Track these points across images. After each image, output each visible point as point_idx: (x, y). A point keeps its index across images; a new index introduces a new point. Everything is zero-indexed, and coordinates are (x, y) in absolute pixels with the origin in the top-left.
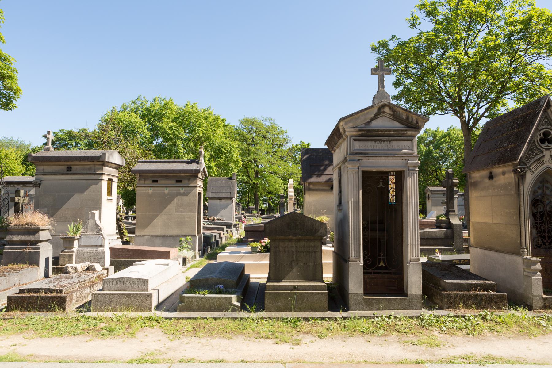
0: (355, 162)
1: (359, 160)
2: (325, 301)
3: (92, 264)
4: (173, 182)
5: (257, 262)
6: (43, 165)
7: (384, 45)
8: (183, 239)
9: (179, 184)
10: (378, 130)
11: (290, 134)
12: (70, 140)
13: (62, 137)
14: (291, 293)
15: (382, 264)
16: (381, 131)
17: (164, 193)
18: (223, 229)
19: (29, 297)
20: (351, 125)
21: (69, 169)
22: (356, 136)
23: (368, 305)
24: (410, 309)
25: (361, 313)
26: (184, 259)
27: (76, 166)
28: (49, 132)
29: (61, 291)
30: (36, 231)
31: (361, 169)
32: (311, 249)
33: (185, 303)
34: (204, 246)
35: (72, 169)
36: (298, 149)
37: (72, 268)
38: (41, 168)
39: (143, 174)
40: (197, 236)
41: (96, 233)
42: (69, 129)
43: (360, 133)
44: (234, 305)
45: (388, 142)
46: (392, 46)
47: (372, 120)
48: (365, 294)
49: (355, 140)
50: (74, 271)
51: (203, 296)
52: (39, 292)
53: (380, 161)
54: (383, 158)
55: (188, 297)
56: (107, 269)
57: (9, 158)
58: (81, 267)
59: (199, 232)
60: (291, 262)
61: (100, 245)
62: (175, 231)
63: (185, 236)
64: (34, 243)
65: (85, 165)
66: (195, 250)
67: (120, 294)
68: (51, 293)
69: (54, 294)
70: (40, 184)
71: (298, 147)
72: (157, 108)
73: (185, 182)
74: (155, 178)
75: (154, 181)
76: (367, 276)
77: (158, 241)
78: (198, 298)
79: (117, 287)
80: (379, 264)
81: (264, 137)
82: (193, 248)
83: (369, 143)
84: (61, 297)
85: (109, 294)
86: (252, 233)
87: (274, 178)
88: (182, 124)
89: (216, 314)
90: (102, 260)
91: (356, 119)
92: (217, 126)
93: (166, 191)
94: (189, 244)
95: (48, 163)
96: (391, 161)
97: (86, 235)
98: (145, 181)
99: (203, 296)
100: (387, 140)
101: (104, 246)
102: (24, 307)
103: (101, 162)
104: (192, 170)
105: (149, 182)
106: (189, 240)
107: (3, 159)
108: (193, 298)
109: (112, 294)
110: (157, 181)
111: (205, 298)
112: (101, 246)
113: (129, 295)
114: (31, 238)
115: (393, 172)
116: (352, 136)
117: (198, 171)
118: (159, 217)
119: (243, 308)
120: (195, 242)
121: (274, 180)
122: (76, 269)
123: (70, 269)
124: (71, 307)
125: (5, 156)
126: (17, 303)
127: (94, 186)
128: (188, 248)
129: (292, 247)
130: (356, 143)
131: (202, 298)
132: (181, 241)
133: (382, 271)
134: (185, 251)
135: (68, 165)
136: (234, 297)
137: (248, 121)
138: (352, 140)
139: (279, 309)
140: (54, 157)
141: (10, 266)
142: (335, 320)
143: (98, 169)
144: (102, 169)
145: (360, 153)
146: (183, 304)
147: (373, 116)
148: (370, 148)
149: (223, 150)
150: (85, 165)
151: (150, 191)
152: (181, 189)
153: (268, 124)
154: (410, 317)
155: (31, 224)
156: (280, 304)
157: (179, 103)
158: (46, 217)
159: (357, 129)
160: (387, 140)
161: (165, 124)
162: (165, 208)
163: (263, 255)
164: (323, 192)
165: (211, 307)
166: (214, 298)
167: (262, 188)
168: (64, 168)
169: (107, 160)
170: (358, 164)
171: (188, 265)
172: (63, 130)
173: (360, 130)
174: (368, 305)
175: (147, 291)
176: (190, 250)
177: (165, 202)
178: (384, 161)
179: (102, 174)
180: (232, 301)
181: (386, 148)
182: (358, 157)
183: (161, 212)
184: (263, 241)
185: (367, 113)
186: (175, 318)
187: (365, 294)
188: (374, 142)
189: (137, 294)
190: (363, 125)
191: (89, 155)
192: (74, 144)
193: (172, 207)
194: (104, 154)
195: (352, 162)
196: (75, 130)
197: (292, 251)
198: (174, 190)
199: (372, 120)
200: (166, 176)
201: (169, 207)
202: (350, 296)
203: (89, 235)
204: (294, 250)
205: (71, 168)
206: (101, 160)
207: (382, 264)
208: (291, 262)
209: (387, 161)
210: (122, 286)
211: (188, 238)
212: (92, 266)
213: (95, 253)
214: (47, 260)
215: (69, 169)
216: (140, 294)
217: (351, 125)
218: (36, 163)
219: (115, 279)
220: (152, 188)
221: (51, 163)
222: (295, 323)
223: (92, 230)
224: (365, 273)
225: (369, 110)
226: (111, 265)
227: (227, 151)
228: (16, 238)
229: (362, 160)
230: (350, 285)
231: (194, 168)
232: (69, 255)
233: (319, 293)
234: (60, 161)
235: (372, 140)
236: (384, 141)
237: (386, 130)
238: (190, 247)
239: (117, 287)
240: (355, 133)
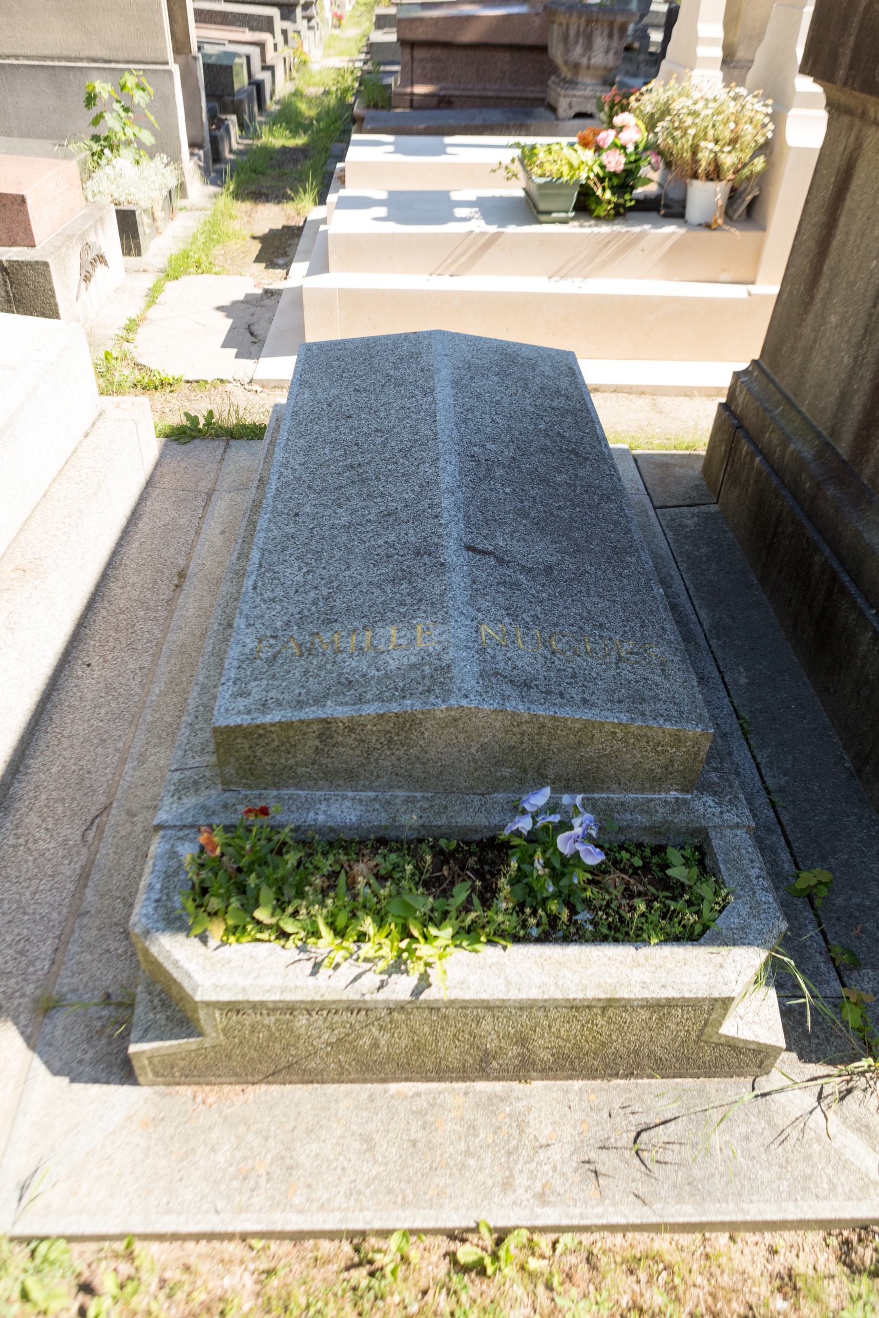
5: (570, 286)
8: (103, 88)
18: (267, 24)
26: (127, 222)
34: (213, 117)
40: (175, 69)
59: (181, 45)
63: (110, 65)
66: (175, 158)
82: (164, 146)
86: (438, 52)
94: (141, 121)
106: (139, 98)
120: (167, 100)
128: (141, 145)
134: (122, 163)
146: (191, 1043)
150: (465, 251)
163: (609, 240)
169: (355, 137)
171: (158, 246)
176: (151, 154)
184: (607, 137)
211: (130, 81)
238: (147, 138)
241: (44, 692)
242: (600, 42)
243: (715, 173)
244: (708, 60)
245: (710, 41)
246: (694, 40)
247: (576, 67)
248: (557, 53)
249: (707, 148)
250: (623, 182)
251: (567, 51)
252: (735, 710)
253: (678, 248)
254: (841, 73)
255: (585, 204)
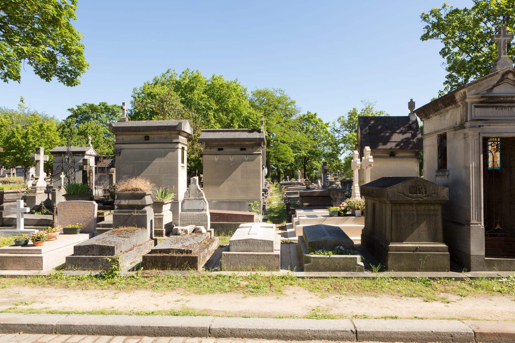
0: (477, 129)
1: (480, 126)
2: (447, 262)
3: (197, 227)
4: (238, 150)
6: (123, 135)
7: (435, 13)
8: (252, 204)
9: (243, 152)
10: (500, 97)
11: (298, 104)
12: (92, 113)
13: (85, 110)
14: (414, 254)
15: (498, 227)
16: (503, 97)
17: (230, 160)
19: (163, 257)
20: (473, 91)
21: (147, 138)
22: (476, 103)
23: (489, 266)
24: (482, 271)
25: (488, 274)
27: (153, 136)
28: (124, 104)
29: (191, 251)
30: (142, 196)
31: (482, 135)
32: (432, 213)
33: (312, 263)
35: (150, 138)
36: (306, 119)
37: (182, 230)
38: (121, 137)
39: (208, 143)
41: (198, 198)
42: (91, 103)
43: (482, 100)
44: (359, 265)
45: (510, 109)
46: (443, 14)
47: (494, 86)
48: (487, 255)
49: (476, 107)
50: (184, 233)
51: (328, 256)
52: (170, 252)
53: (501, 127)
54: (505, 124)
55: (314, 258)
56: (210, 231)
57: (50, 130)
58: (190, 228)
60: (412, 225)
61: (202, 209)
62: (241, 197)
64: (141, 207)
65: (162, 134)
67: (249, 255)
68: (182, 253)
69: (185, 255)
70: (120, 153)
71: (305, 117)
72: (187, 81)
73: (249, 150)
74: (219, 146)
75: (242, 149)
76: (489, 238)
77: (224, 205)
78: (324, 258)
79: (243, 247)
80: (496, 226)
81: (276, 108)
83: (490, 110)
84: (192, 257)
85: (239, 255)
87: (284, 147)
88: (211, 96)
89: (343, 274)
90: (205, 223)
91: (479, 86)
92: (244, 98)
93: (231, 158)
95: (128, 133)
96: (511, 127)
97: (188, 199)
98: (210, 149)
99: (328, 256)
100: (508, 107)
101: (206, 210)
102: (158, 266)
103: (177, 130)
104: (256, 139)
105: (214, 150)
107: (45, 131)
108: (319, 258)
109: (241, 255)
110: (222, 149)
111: (331, 258)
112: (203, 210)
113: (258, 255)
114: (138, 202)
115: (497, 138)
116: (472, 103)
117: (262, 140)
118: (225, 183)
119: (368, 268)
121: (285, 149)
122: (186, 232)
123: (180, 232)
124: (201, 265)
125: (47, 128)
126: (152, 263)
127: (171, 153)
129: (413, 210)
130: (477, 110)
131: (328, 258)
132: (250, 205)
133: (499, 234)
135: (146, 135)
136: (358, 257)
137: (260, 93)
138: (473, 107)
139: (402, 269)
140: (133, 127)
141: (121, 228)
142: (462, 279)
143: (175, 138)
144: (178, 138)
145: (481, 120)
147: (496, 82)
148: (491, 115)
149: (250, 120)
150: (162, 134)
151: (216, 158)
152: (245, 156)
153: (278, 95)
154: (299, 277)
155: (137, 189)
156: (403, 264)
157: (206, 76)
158: (148, 183)
159: (480, 95)
160: (508, 107)
161: (197, 95)
162: (231, 174)
164: (382, 159)
165: (336, 267)
166: (339, 258)
167: (274, 157)
168: (142, 137)
170: (479, 130)
172: (86, 104)
173: (482, 97)
174: (489, 266)
175: (273, 252)
177: (231, 168)
178: (505, 127)
179: (178, 143)
180: (356, 262)
181: (508, 114)
182: (479, 123)
183: (226, 179)
185: (491, 80)
186: (307, 277)
187: (487, 255)
188: (495, 109)
189: (265, 255)
190: (485, 92)
191: (166, 125)
192: (95, 117)
193: (237, 173)
194: (180, 124)
195: (474, 129)
196: (96, 104)
197: (413, 214)
198: (239, 157)
199: (494, 86)
200: (231, 144)
201: (234, 173)
202: (471, 258)
203: (192, 200)
204: (415, 213)
205: (148, 137)
206: (178, 129)
207: (498, 227)
208: (412, 225)
209: (508, 127)
210: (248, 247)
212: (199, 229)
213: (198, 217)
214: (151, 221)
215: (147, 138)
216: (268, 255)
217: (473, 91)
218: (116, 133)
219: (241, 240)
220: (218, 156)
221: (130, 133)
222: (426, 282)
223: (194, 195)
224: (486, 235)
225: (493, 77)
226: (211, 228)
227: (254, 121)
228: (124, 202)
229: (483, 126)
230: (471, 246)
231: (258, 137)
232: (159, 218)
233: (441, 254)
234: (139, 131)
235: (493, 107)
236: (505, 107)
237: (509, 97)
239: (243, 247)
240: (476, 100)
241: (414, 333)
242: (340, 194)
243: (358, 209)
244: (358, 196)
245: (358, 193)
246: (355, 193)
247: (336, 198)
248: (332, 197)
249: (356, 206)
250: (345, 211)
251: (334, 196)
252: (477, 320)
253: (354, 220)
254: (477, 246)
255: (339, 214)
